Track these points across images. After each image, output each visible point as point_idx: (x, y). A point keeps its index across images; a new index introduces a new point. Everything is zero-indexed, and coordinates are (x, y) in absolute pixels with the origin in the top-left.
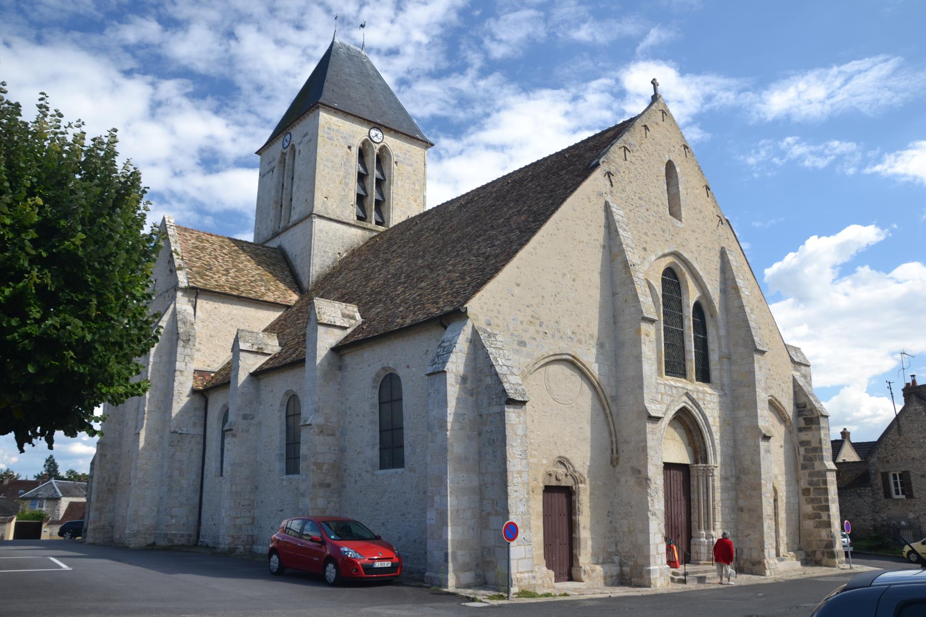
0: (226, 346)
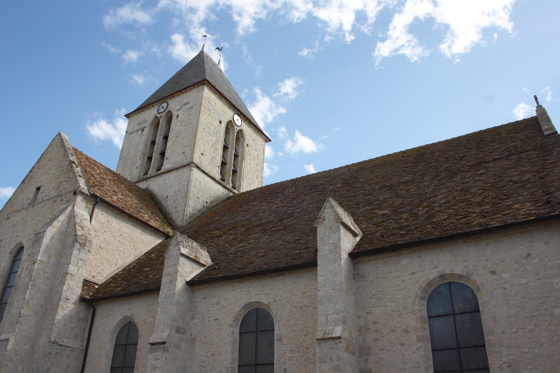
0: (111, 261)
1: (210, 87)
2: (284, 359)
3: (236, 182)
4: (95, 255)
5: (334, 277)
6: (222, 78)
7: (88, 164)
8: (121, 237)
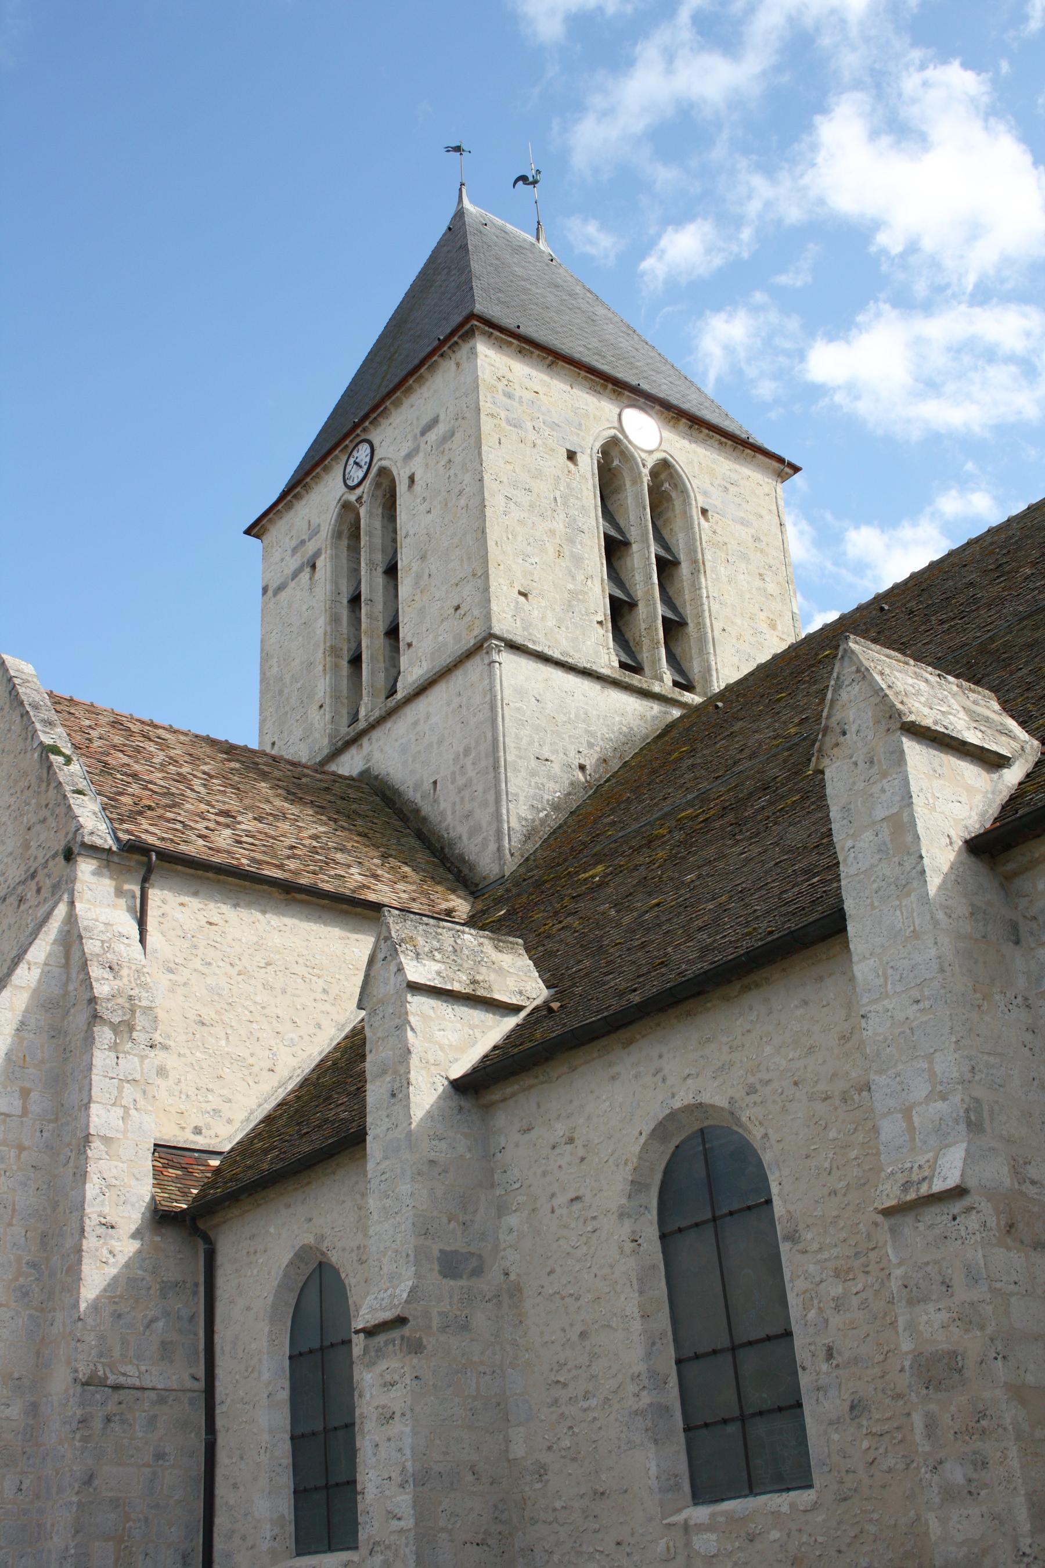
0: (251, 1061)
1: (496, 338)
2: (820, 1308)
3: (691, 662)
4: (187, 1052)
5: (909, 954)
6: (557, 286)
7: (118, 740)
8: (269, 967)
